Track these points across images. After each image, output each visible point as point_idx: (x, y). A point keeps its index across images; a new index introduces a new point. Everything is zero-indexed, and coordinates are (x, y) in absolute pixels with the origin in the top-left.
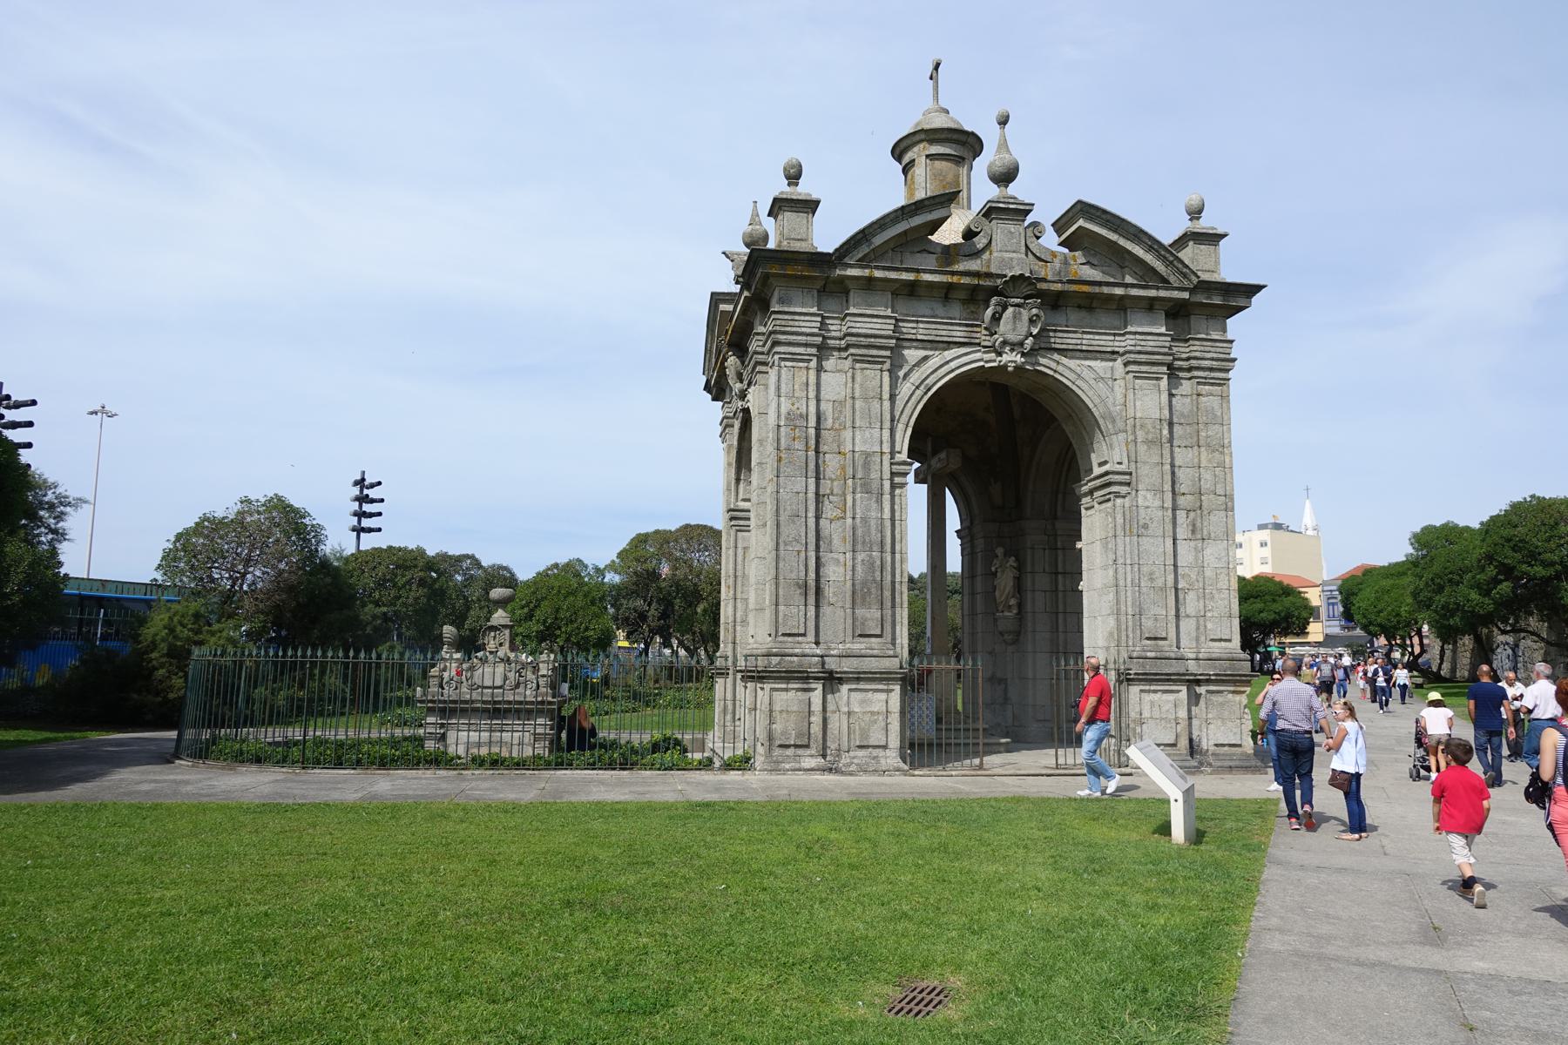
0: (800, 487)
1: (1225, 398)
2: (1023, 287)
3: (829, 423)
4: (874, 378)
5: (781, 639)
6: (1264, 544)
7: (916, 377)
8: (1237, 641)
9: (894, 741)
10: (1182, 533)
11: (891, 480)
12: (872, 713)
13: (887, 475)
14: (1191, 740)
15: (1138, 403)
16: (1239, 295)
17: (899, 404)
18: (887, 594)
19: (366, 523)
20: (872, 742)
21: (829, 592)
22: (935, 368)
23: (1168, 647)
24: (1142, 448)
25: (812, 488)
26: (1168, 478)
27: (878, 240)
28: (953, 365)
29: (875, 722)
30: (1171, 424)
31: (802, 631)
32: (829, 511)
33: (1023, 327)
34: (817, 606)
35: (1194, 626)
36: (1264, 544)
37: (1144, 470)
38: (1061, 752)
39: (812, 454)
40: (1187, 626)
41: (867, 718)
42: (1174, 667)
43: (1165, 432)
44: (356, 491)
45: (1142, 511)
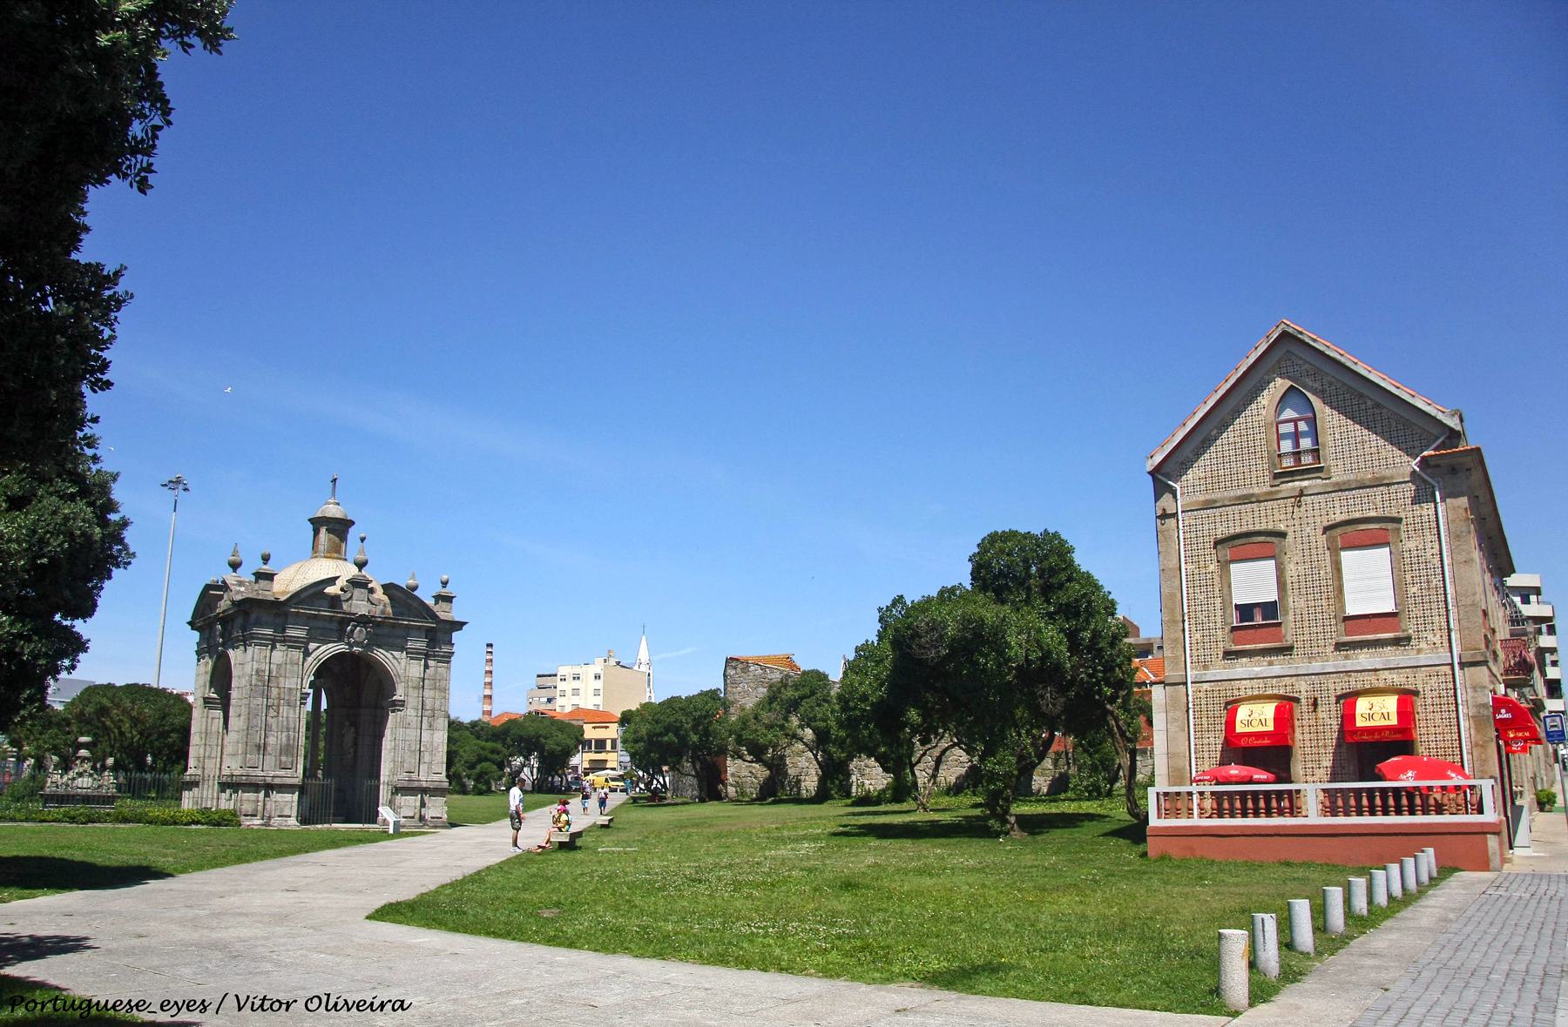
2: (363, 620)
4: (297, 655)
6: (597, 677)
7: (314, 655)
9: (294, 813)
16: (460, 625)
22: (324, 651)
23: (414, 776)
36: (597, 677)
42: (416, 784)
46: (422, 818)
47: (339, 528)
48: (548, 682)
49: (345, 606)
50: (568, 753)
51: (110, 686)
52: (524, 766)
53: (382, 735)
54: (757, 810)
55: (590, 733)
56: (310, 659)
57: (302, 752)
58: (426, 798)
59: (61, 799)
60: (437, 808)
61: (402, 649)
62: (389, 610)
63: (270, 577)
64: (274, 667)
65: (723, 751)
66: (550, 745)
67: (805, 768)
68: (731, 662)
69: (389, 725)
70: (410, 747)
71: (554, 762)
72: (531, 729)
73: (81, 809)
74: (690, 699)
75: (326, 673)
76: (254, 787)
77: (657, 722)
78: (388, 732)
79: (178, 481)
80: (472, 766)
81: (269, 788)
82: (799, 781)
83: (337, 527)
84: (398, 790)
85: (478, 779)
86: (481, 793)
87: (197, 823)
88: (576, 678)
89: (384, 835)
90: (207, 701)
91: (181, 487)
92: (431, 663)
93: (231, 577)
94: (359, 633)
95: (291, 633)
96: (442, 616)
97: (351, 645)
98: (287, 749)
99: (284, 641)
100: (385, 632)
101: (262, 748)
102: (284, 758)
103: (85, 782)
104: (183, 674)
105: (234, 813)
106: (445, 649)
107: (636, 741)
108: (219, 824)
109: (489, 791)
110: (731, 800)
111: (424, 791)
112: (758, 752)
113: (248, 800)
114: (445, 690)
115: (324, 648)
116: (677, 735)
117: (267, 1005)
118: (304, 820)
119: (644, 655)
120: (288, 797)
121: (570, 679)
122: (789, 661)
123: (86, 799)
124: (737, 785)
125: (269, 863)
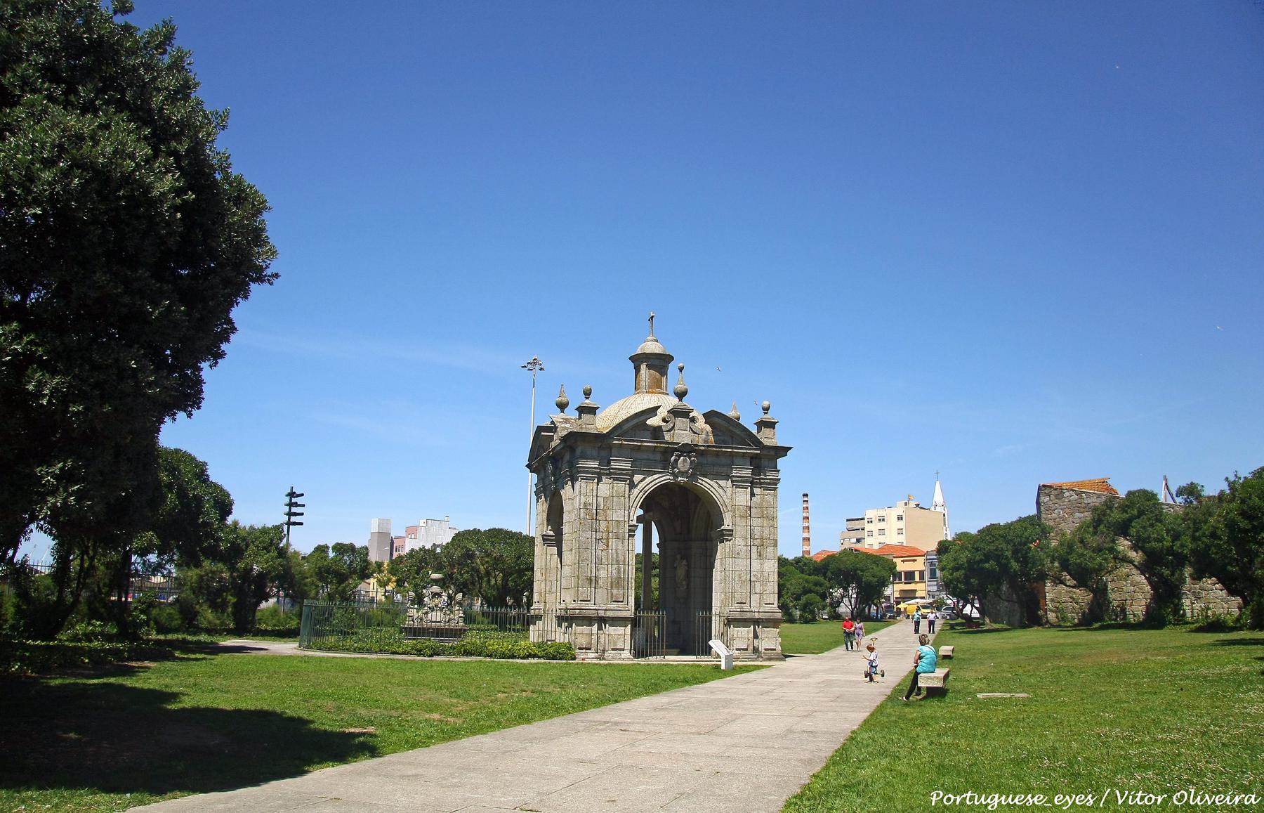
1: (776, 496)
2: (686, 449)
4: (623, 487)
6: (900, 518)
7: (640, 487)
9: (628, 647)
16: (783, 451)
19: (293, 519)
22: (648, 482)
27: (625, 427)
36: (900, 518)
37: (739, 528)
40: (755, 598)
42: (748, 616)
44: (287, 500)
46: (756, 650)
47: (659, 363)
48: (856, 525)
49: (667, 437)
50: (884, 583)
51: (476, 532)
52: (843, 597)
53: (712, 567)
54: (1085, 636)
55: (901, 566)
56: (636, 491)
57: (632, 584)
58: (759, 630)
59: (415, 632)
60: (770, 639)
61: (727, 477)
62: (711, 438)
63: (592, 411)
64: (601, 500)
65: (1042, 577)
66: (867, 577)
67: (1132, 591)
68: (1042, 489)
69: (718, 555)
70: (741, 578)
71: (870, 592)
72: (849, 563)
73: (432, 642)
74: (1009, 526)
75: (650, 503)
76: (587, 620)
77: (977, 550)
78: (717, 563)
79: (535, 362)
80: (798, 598)
81: (602, 621)
82: (1123, 610)
83: (657, 362)
84: (729, 622)
85: (803, 609)
86: (807, 622)
87: (534, 656)
88: (882, 520)
89: (716, 672)
90: (545, 538)
91: (538, 367)
92: (757, 491)
93: (558, 417)
94: (684, 463)
95: (614, 465)
96: (766, 442)
97: (675, 475)
98: (618, 582)
99: (609, 475)
100: (710, 460)
101: (593, 581)
102: (615, 591)
103: (436, 616)
104: (520, 513)
105: (569, 647)
106: (770, 475)
107: (956, 569)
108: (554, 658)
109: (813, 620)
110: (1053, 626)
111: (756, 622)
112: (1083, 577)
113: (581, 634)
114: (773, 518)
115: (649, 479)
116: (999, 563)
118: (638, 652)
119: (938, 497)
120: (620, 630)
121: (875, 521)
122: (1104, 484)
123: (439, 633)
124: (1057, 610)
125: (537, 728)
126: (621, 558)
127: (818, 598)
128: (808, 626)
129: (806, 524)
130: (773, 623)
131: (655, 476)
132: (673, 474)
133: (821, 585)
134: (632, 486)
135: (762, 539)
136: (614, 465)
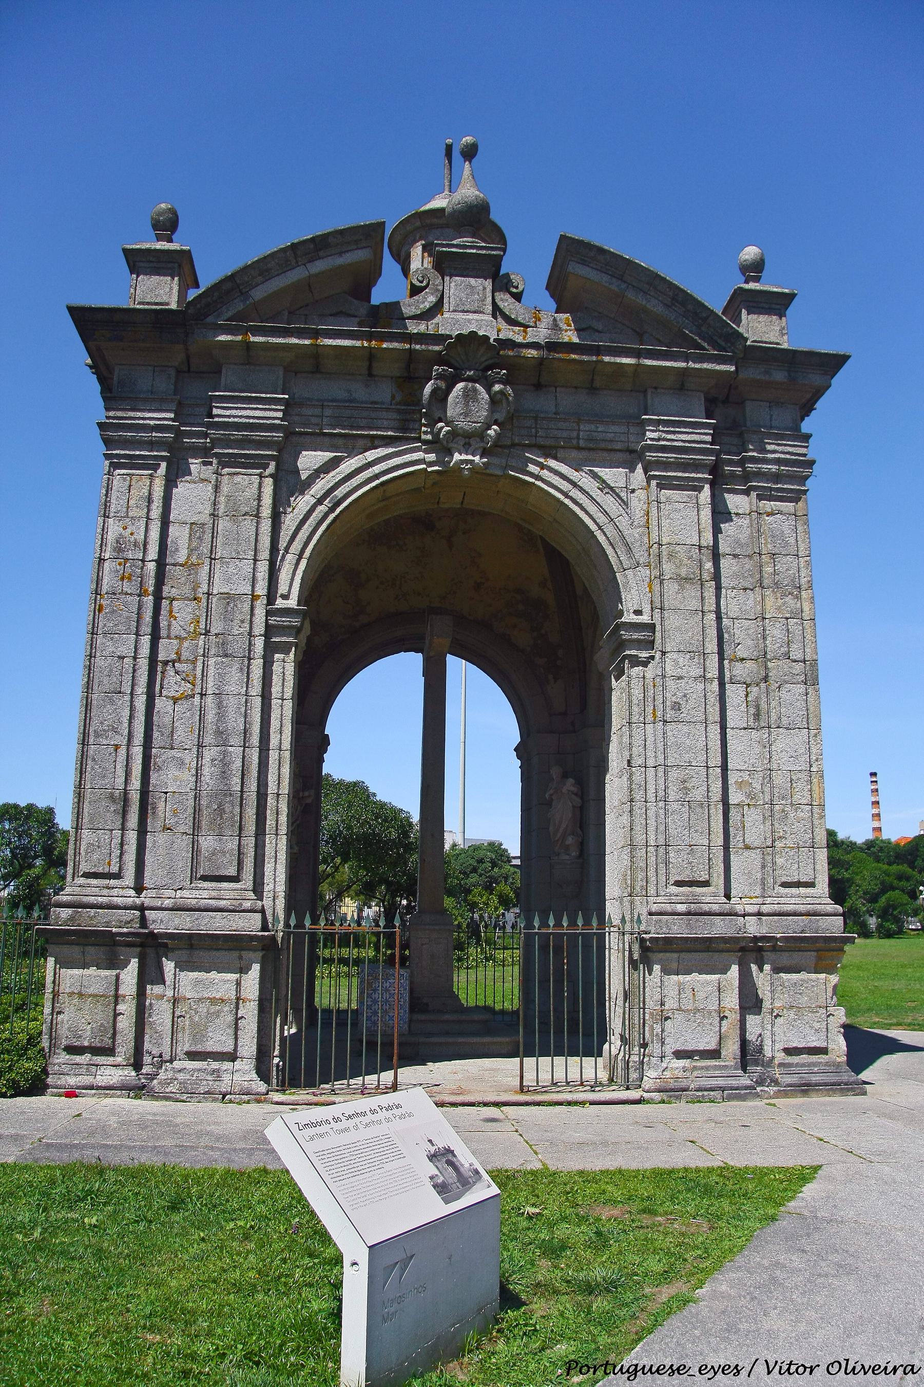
0: (127, 649)
2: (470, 356)
3: (182, 556)
4: (252, 487)
5: (82, 881)
8: (823, 886)
9: (248, 1046)
10: (734, 718)
11: (267, 635)
12: (213, 1001)
13: (259, 628)
14: (744, 1043)
15: (665, 523)
17: (289, 522)
18: (251, 813)
20: (211, 1046)
21: (163, 809)
22: (347, 475)
23: (711, 897)
24: (671, 588)
25: (145, 650)
26: (712, 633)
28: (377, 469)
29: (218, 1014)
30: (716, 557)
31: (115, 869)
32: (172, 683)
33: (481, 410)
34: (142, 832)
35: (758, 864)
37: (673, 621)
38: (529, 1062)
39: (149, 600)
41: (203, 1008)
42: (719, 928)
43: (709, 565)
45: (670, 683)
46: (749, 1054)
56: (303, 503)
58: (762, 978)
60: (803, 1013)
61: (630, 457)
80: (874, 899)
85: (884, 915)
86: (889, 935)
92: (736, 502)
94: (467, 405)
100: (552, 400)
111: (751, 951)
117: (793, 1368)
120: (221, 983)
126: (235, 723)
127: (906, 898)
128: (892, 941)
129: (875, 811)
130: (819, 953)
131: (371, 455)
132: (434, 444)
133: (908, 879)
134: (288, 484)
135: (763, 658)
136: (222, 413)
